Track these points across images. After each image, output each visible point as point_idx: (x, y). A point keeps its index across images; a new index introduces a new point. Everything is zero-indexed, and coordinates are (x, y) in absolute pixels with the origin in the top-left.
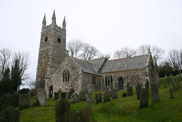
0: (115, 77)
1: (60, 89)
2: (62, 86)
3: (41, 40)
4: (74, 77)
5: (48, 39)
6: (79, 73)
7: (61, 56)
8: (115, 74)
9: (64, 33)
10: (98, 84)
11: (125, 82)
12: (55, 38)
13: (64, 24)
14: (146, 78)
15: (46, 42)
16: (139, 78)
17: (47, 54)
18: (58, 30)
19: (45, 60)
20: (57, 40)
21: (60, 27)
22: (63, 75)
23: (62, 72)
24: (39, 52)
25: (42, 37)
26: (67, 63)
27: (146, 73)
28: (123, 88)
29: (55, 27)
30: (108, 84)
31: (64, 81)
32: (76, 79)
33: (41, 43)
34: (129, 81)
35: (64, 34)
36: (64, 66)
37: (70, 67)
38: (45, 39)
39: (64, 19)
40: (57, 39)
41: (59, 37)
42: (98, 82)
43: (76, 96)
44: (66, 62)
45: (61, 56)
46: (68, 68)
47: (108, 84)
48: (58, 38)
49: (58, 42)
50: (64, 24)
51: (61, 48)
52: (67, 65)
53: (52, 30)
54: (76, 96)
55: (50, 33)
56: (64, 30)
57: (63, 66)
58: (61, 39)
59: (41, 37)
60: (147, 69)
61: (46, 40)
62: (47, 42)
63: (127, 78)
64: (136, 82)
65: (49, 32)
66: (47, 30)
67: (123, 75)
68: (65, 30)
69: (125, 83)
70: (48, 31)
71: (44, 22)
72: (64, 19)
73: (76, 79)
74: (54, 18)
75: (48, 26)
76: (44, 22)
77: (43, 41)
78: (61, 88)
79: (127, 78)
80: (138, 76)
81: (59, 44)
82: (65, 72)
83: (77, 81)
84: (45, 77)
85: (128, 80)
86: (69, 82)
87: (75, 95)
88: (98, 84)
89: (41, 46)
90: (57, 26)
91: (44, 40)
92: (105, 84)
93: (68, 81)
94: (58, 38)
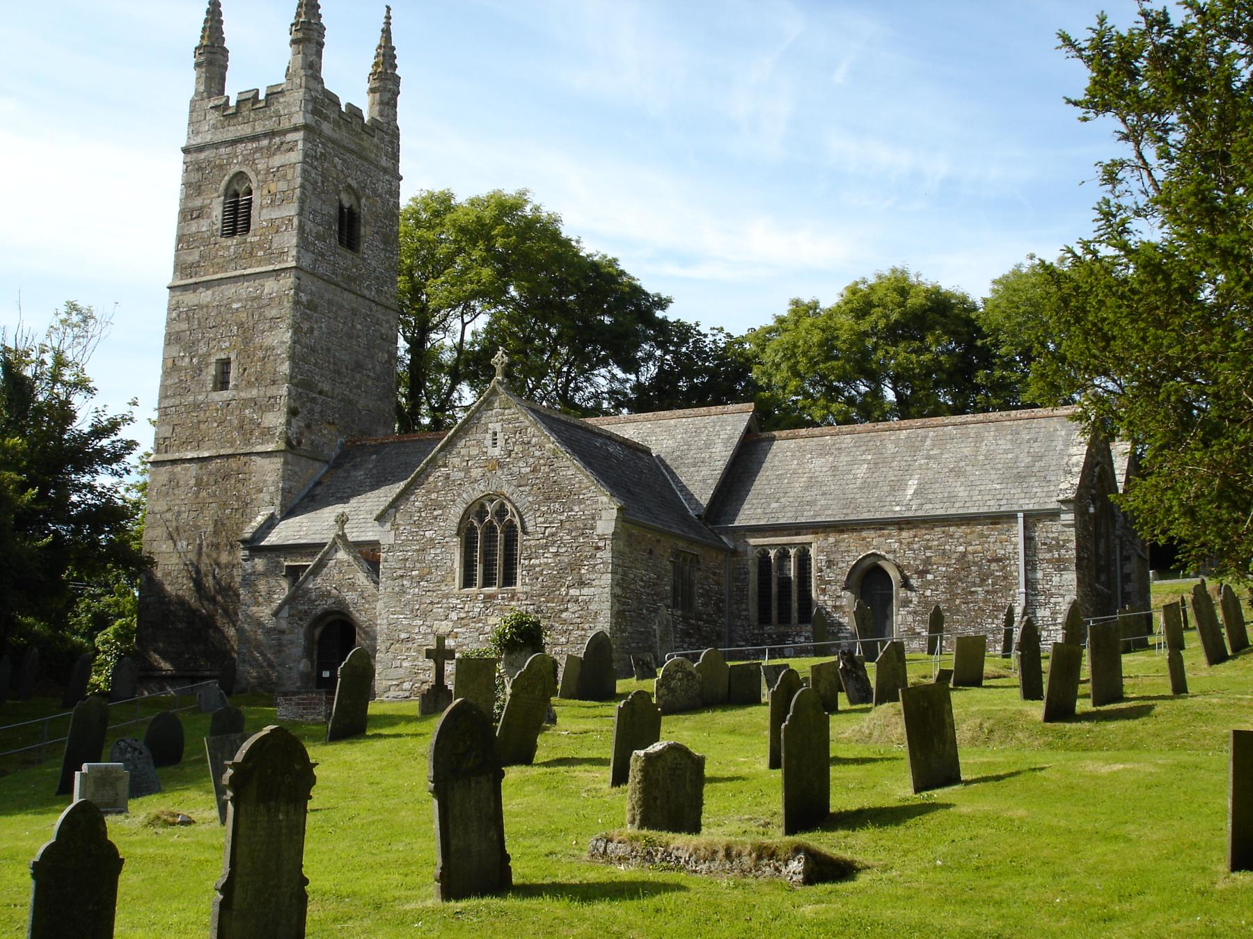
0: (830, 563)
1: (441, 640)
2: (454, 616)
3: (188, 214)
4: (556, 554)
5: (260, 217)
6: (593, 528)
7: (358, 366)
8: (837, 543)
9: (384, 162)
10: (710, 610)
11: (906, 603)
12: (318, 205)
13: (386, 79)
14: (1056, 579)
15: (234, 233)
16: (1005, 578)
17: (247, 341)
18: (342, 135)
19: (226, 395)
20: (335, 227)
21: (354, 112)
22: (466, 534)
23: (456, 512)
24: (170, 322)
25: (193, 187)
26: (496, 452)
27: (1059, 547)
28: (649, 673)
29: (315, 112)
30: (774, 613)
31: (468, 581)
32: (574, 566)
33: (180, 239)
34: (936, 595)
35: (385, 171)
36: (476, 473)
37: (521, 482)
38: (222, 206)
39: (387, 33)
40: (333, 212)
41: (347, 201)
42: (706, 594)
43: (680, 675)
44: (489, 442)
45: (358, 366)
46: (506, 490)
47: (774, 613)
48: (341, 208)
49: (341, 242)
50: (386, 79)
51: (366, 293)
52: (501, 465)
53: (290, 137)
54: (680, 675)
55: (277, 160)
56: (384, 134)
57: (467, 470)
58: (364, 212)
59: (187, 185)
60: (1069, 518)
61: (238, 217)
62: (250, 238)
63: (922, 573)
64: (985, 601)
65: (270, 152)
66: (246, 130)
67: (887, 546)
68: (395, 135)
69: (903, 612)
70: (255, 138)
71: (212, 55)
72: (387, 33)
73: (574, 566)
74: (309, 33)
75: (250, 100)
76: (212, 55)
77: (204, 226)
78: (444, 627)
79: (922, 573)
80: (998, 560)
81: (345, 259)
82: (481, 513)
83: (582, 584)
84: (248, 532)
85: (926, 585)
86: (519, 587)
87: (676, 672)
88: (705, 604)
89: (181, 267)
90: (334, 100)
91: (217, 211)
92: (753, 609)
93: (509, 580)
94: (341, 208)
